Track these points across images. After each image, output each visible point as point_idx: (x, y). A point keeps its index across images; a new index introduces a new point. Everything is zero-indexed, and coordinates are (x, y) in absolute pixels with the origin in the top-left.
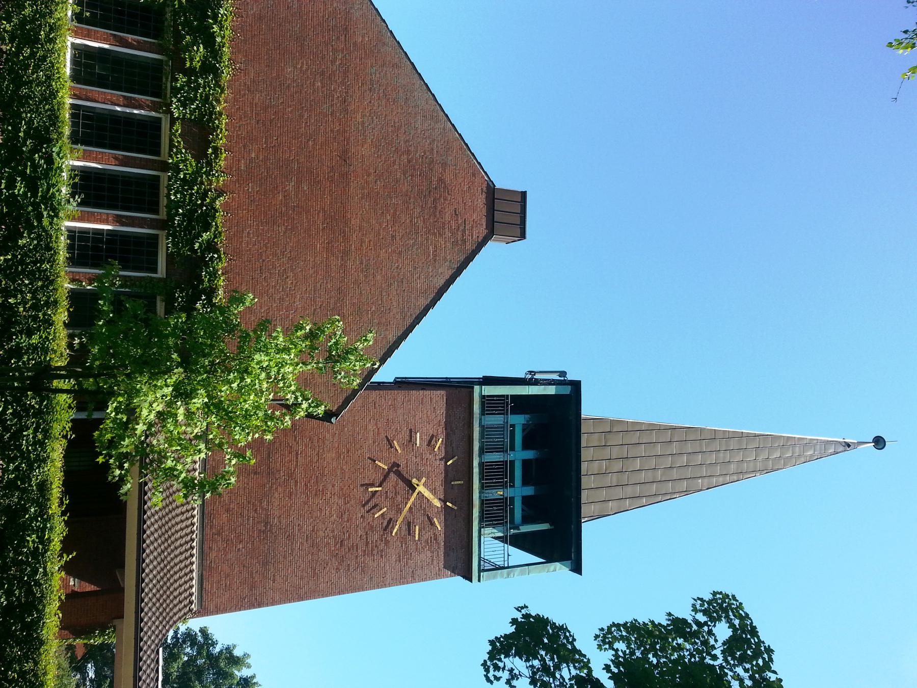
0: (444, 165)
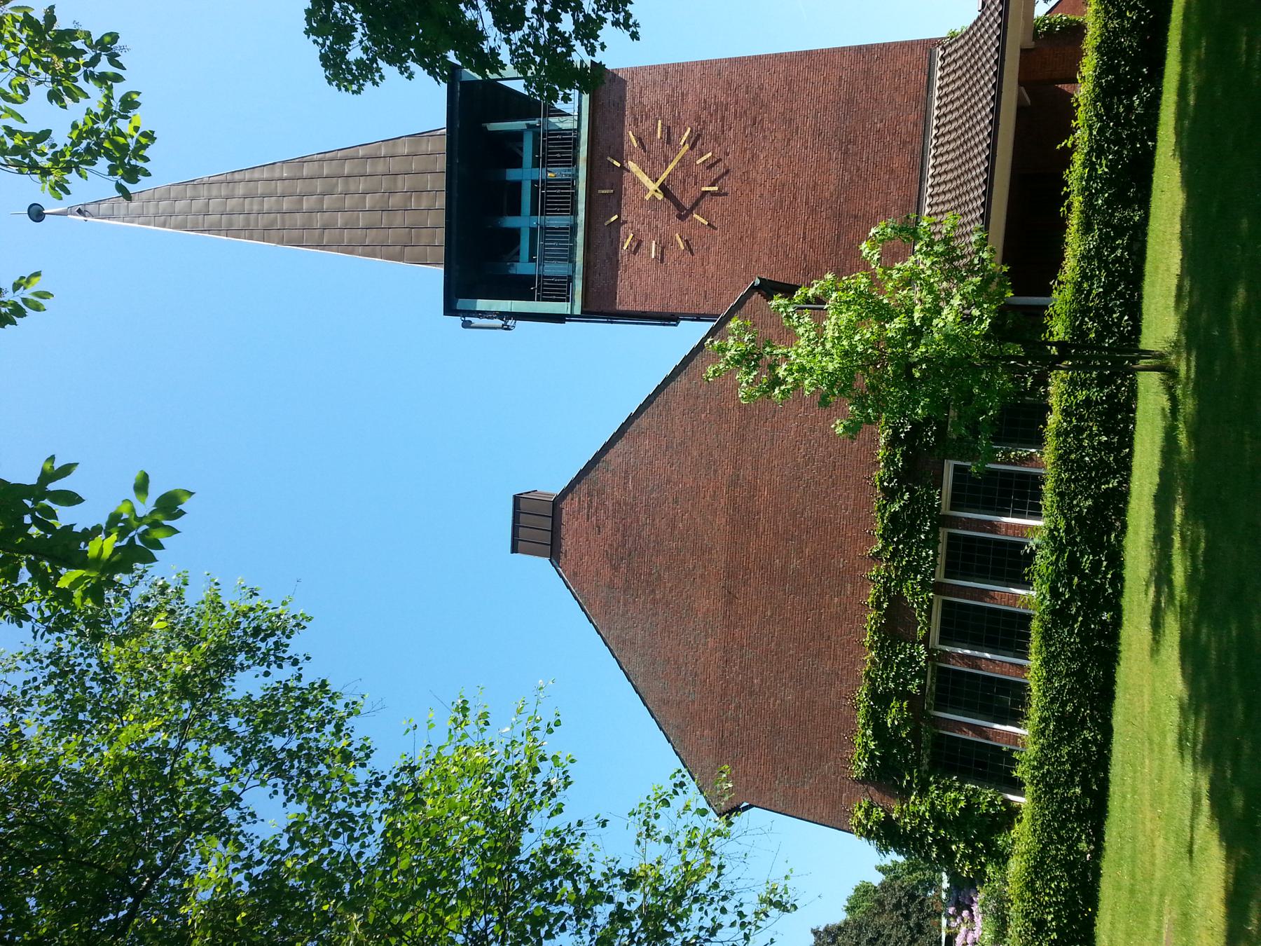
0: (611, 586)
